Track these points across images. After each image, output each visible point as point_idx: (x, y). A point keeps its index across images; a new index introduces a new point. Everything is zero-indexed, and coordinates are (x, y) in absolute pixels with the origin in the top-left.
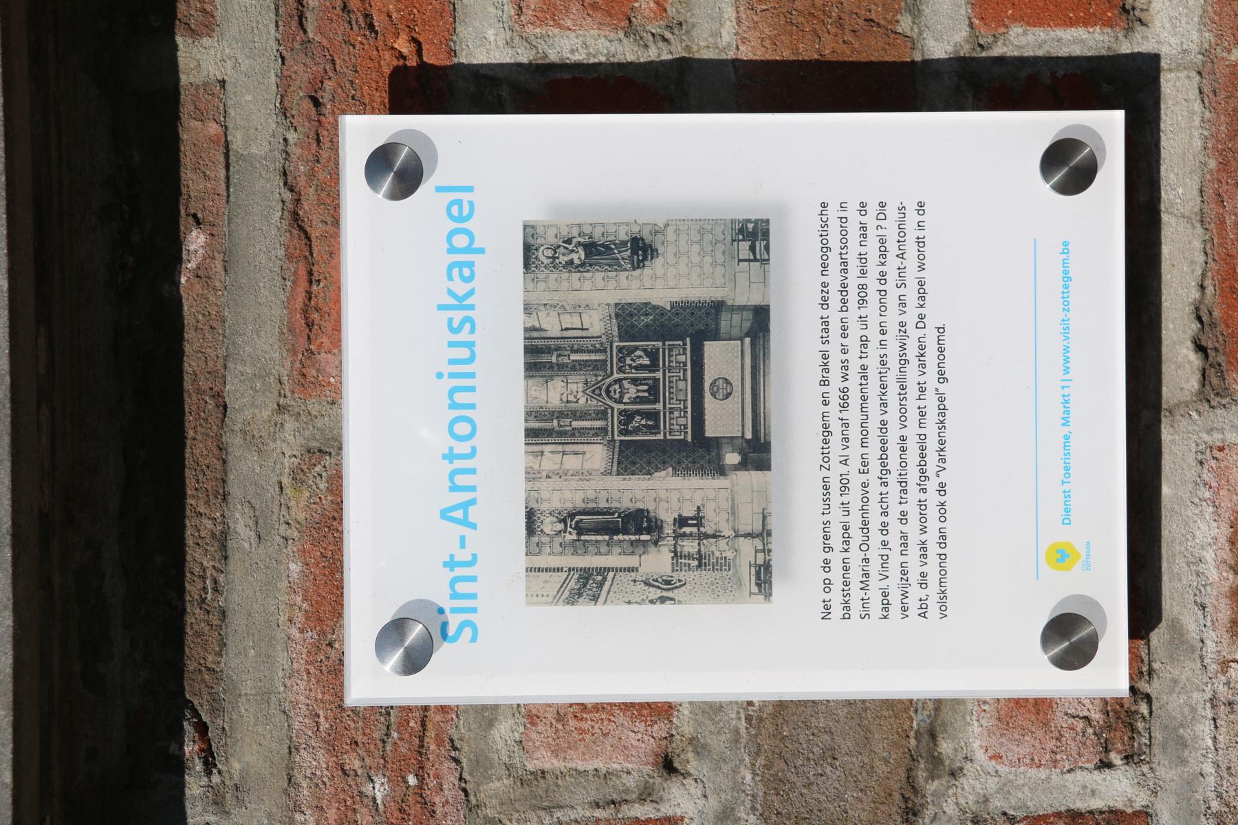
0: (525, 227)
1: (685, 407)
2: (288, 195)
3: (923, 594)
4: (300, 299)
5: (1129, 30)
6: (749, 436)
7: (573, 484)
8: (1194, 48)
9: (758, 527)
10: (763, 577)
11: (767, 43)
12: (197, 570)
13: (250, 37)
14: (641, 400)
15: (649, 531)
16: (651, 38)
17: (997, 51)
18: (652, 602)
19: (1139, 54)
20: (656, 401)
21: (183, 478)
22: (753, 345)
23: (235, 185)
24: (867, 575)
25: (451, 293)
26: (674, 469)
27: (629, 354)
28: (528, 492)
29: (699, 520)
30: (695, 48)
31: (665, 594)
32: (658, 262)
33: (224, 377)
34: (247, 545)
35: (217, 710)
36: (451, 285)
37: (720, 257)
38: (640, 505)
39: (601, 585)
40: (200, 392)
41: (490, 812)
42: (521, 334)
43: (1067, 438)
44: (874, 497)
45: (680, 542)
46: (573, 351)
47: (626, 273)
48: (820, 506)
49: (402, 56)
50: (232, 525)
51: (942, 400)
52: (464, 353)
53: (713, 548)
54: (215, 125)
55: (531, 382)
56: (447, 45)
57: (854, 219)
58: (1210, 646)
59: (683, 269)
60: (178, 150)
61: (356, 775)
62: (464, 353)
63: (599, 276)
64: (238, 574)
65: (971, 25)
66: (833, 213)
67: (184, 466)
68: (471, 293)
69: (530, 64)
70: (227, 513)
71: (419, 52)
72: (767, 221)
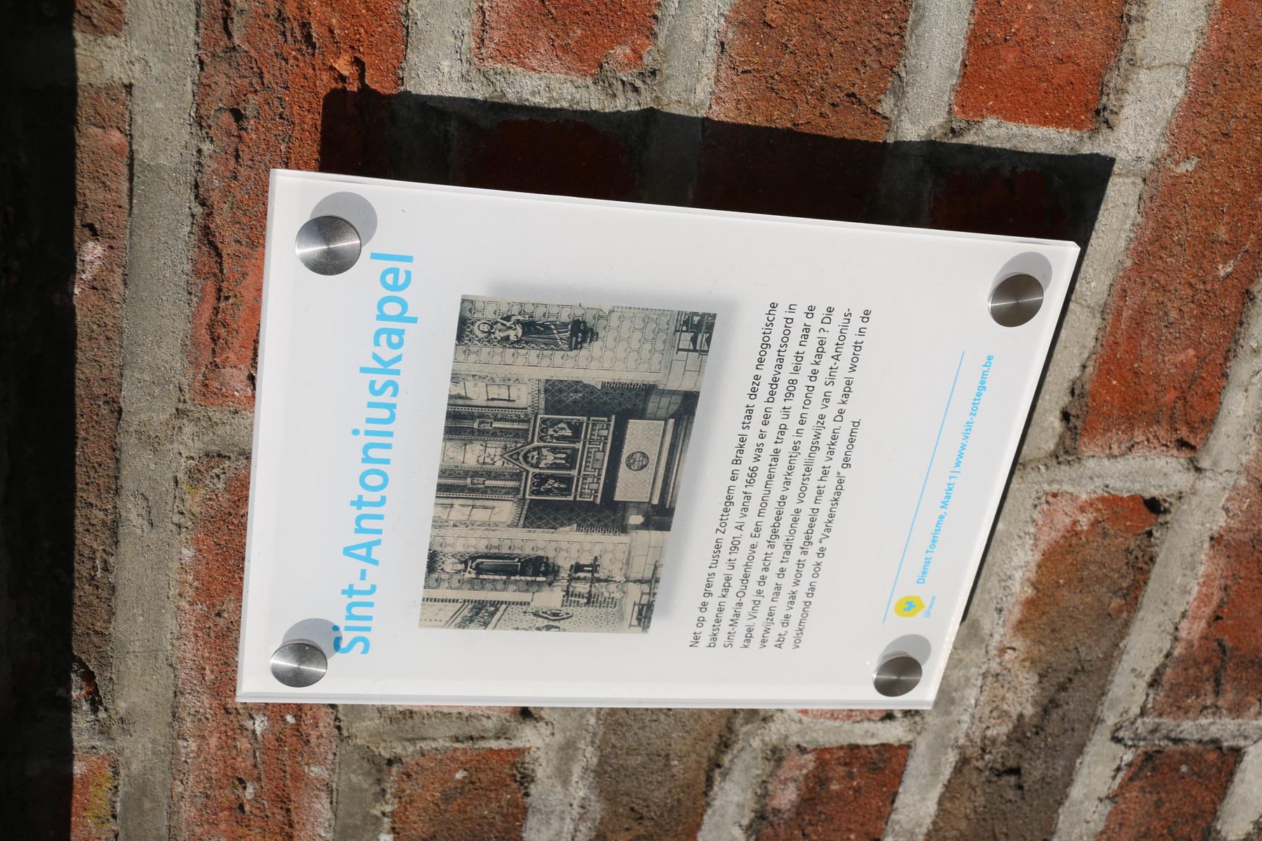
0: (463, 301)
1: (599, 475)
2: (198, 210)
3: (782, 631)
4: (206, 316)
5: (1096, 131)
6: (655, 501)
7: (479, 533)
8: (1148, 157)
9: (648, 575)
10: (644, 615)
11: (742, 106)
12: (86, 552)
13: (165, 38)
14: (555, 466)
15: (545, 574)
16: (621, 88)
17: (968, 139)
18: (538, 629)
19: (1097, 154)
20: (567, 462)
21: (74, 474)
22: (676, 426)
23: (140, 195)
24: (737, 615)
25: (376, 357)
26: (579, 525)
27: (552, 426)
28: (433, 537)
29: (594, 567)
30: (665, 101)
31: (551, 623)
32: (597, 345)
33: (120, 384)
34: (139, 532)
35: (105, 662)
36: (377, 350)
37: (659, 346)
38: (541, 553)
39: (492, 614)
40: (95, 398)
41: (359, 742)
42: (446, 401)
43: (941, 517)
44: (760, 555)
45: (573, 584)
46: (496, 419)
47: (562, 353)
48: (710, 561)
49: (343, 78)
50: (123, 514)
51: (840, 482)
52: (385, 414)
53: (604, 590)
54: (118, 134)
55: (449, 444)
56: (395, 74)
57: (800, 319)
58: (997, 637)
59: (621, 353)
60: (74, 157)
61: (238, 713)
62: (385, 414)
63: (534, 353)
64: (129, 554)
65: (950, 112)
66: (781, 314)
67: (74, 464)
68: (399, 358)
69: (485, 102)
70: (119, 504)
71: (362, 77)
72: (714, 316)
